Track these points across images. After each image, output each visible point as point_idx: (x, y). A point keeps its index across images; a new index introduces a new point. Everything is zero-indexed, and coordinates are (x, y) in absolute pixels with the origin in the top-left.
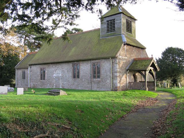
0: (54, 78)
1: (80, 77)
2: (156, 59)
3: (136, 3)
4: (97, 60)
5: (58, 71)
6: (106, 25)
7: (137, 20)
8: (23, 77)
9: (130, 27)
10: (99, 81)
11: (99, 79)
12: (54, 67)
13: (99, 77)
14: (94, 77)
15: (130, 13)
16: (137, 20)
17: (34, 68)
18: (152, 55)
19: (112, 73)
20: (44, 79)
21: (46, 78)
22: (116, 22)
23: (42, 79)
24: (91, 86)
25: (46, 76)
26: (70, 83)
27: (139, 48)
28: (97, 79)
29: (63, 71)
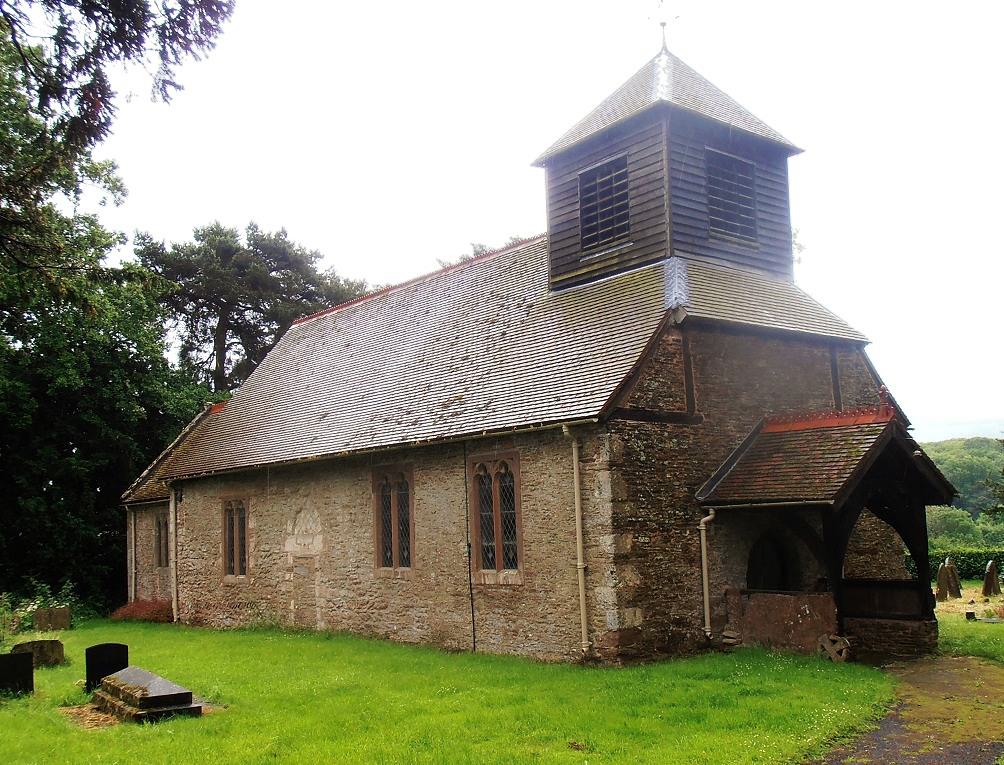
0: (291, 560)
1: (416, 558)
7: (803, 151)
8: (160, 561)
9: (744, 191)
11: (510, 575)
13: (512, 562)
14: (489, 563)
15: (699, 70)
16: (803, 151)
18: (440, 262)
19: (585, 533)
22: (631, 177)
23: (231, 571)
24: (470, 618)
26: (366, 598)
28: (502, 575)
29: (330, 524)
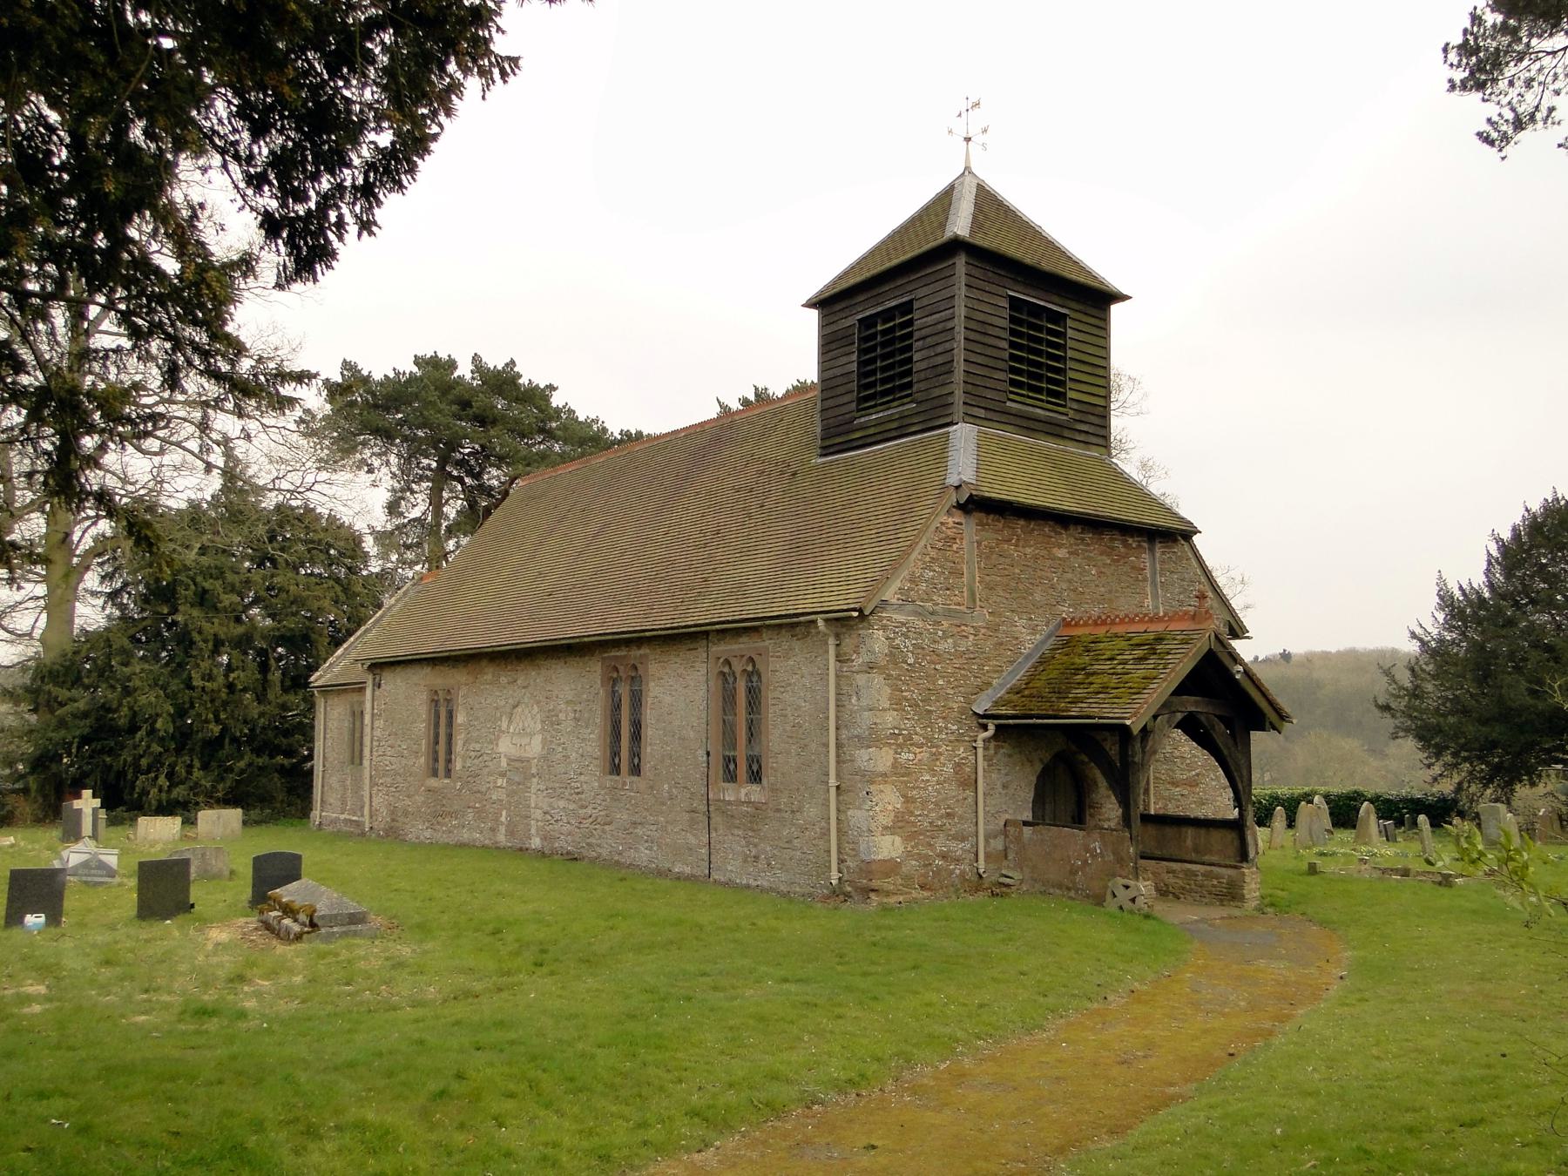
1: (646, 767)
2: (1461, 588)
3: (1535, 130)
4: (744, 639)
5: (529, 718)
6: (854, 357)
10: (757, 806)
12: (504, 680)
16: (1119, 297)
17: (395, 683)
19: (839, 746)
20: (448, 773)
21: (458, 765)
22: (917, 324)
24: (706, 840)
25: (650, 732)
27: (1126, 529)
28: (743, 791)
